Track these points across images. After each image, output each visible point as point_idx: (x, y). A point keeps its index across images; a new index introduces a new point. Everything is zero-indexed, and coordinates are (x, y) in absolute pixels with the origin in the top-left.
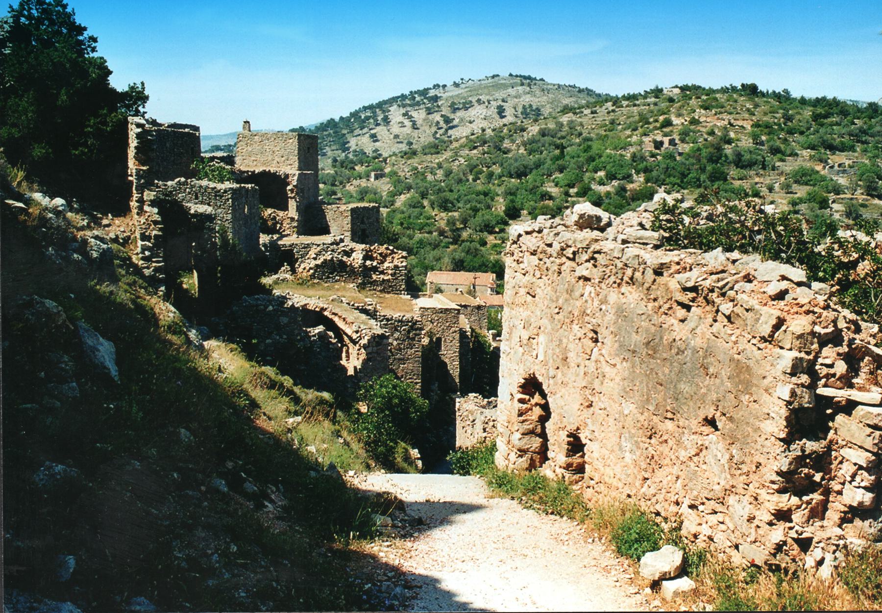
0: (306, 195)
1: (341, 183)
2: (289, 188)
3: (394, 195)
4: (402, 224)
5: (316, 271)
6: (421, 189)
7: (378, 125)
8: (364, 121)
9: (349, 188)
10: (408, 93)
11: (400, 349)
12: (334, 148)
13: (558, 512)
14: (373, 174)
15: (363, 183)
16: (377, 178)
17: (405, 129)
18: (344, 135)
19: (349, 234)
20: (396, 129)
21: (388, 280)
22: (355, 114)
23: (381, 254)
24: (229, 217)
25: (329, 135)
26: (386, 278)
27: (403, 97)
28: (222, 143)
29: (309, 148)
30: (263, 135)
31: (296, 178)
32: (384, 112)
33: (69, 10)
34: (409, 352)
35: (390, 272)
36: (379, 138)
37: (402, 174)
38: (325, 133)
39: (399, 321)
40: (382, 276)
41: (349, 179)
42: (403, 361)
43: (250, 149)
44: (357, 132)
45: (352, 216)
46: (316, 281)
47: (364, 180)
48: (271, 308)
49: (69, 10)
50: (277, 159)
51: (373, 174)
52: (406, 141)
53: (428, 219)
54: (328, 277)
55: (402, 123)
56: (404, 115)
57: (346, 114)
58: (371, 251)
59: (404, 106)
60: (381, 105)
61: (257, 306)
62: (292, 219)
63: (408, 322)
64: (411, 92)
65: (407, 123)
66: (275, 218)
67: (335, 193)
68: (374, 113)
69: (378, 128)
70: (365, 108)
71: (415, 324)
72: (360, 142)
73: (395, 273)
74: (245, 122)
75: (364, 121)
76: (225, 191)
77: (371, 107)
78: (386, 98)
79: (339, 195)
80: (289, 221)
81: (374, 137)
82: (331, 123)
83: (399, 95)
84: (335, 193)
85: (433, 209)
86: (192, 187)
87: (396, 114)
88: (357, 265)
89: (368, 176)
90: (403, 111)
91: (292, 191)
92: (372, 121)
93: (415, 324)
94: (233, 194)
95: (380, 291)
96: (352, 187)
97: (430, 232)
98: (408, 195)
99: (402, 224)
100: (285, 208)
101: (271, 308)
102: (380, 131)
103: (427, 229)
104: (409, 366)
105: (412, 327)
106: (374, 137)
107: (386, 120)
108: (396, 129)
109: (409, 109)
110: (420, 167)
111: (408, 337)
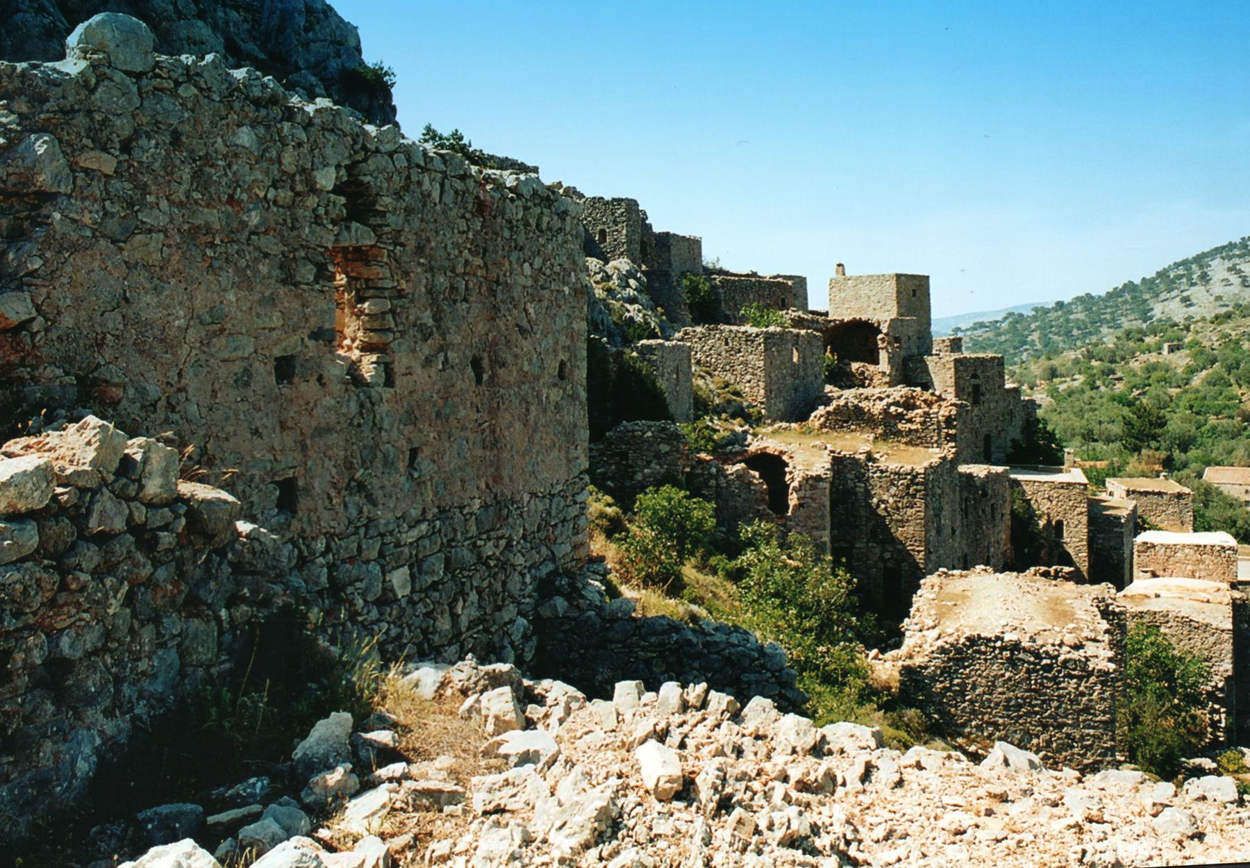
0: (904, 346)
1: (1123, 359)
2: (880, 336)
3: (1192, 371)
4: (1191, 407)
5: (827, 419)
6: (1229, 362)
7: (1193, 284)
8: (1173, 282)
9: (1134, 365)
10: (1238, 240)
11: (898, 509)
12: (1132, 317)
13: (486, 564)
14: (1166, 346)
15: (1153, 358)
16: (1171, 350)
17: (1231, 288)
18: (1146, 300)
19: (952, 390)
20: (1217, 289)
21: (917, 431)
22: (1162, 275)
23: (925, 401)
24: (761, 364)
25: (1125, 302)
26: (914, 427)
27: (1231, 246)
28: (986, 320)
29: (914, 291)
30: (857, 279)
31: (887, 325)
32: (1201, 267)
33: (465, 141)
34: (909, 511)
35: (918, 420)
36: (1194, 301)
37: (1206, 343)
38: (1120, 300)
39: (896, 473)
40: (909, 425)
41: (1134, 353)
42: (902, 523)
43: (843, 295)
44: (1163, 296)
45: (956, 368)
46: (825, 430)
47: (1154, 354)
48: (649, 434)
49: (465, 141)
50: (873, 305)
51: (1166, 346)
52: (1232, 304)
53: (1232, 399)
54: (842, 427)
55: (1227, 280)
56: (1230, 269)
57: (1150, 274)
58: (913, 397)
59: (1230, 258)
60: (1200, 259)
61: (634, 431)
62: (884, 373)
63: (907, 474)
64: (1243, 239)
65: (1235, 279)
66: (863, 373)
67: (1113, 372)
68: (1189, 269)
69: (1193, 289)
70: (1177, 265)
71: (915, 477)
72: (1168, 308)
73: (925, 422)
74: (839, 265)
75: (1173, 282)
76: (757, 335)
77: (1185, 263)
78: (1207, 250)
79: (1119, 374)
80: (879, 376)
81: (1186, 301)
82: (1130, 287)
83: (1226, 243)
84: (1113, 372)
85: (1240, 386)
86: (722, 332)
87: (1218, 268)
88: (876, 412)
89: (1159, 349)
90: (1228, 264)
91: (882, 339)
92: (1184, 280)
93: (915, 477)
94: (766, 339)
95: (906, 443)
96: (1137, 364)
97: (1231, 417)
98: (1210, 371)
99: (1191, 407)
100: (875, 361)
101: (649, 434)
102: (1197, 293)
103: (1226, 412)
104: (910, 529)
105: (911, 480)
106: (1186, 301)
107: (1205, 278)
108: (1217, 289)
109: (1237, 261)
110: (1233, 333)
111: (908, 494)
